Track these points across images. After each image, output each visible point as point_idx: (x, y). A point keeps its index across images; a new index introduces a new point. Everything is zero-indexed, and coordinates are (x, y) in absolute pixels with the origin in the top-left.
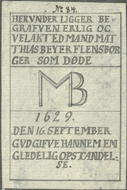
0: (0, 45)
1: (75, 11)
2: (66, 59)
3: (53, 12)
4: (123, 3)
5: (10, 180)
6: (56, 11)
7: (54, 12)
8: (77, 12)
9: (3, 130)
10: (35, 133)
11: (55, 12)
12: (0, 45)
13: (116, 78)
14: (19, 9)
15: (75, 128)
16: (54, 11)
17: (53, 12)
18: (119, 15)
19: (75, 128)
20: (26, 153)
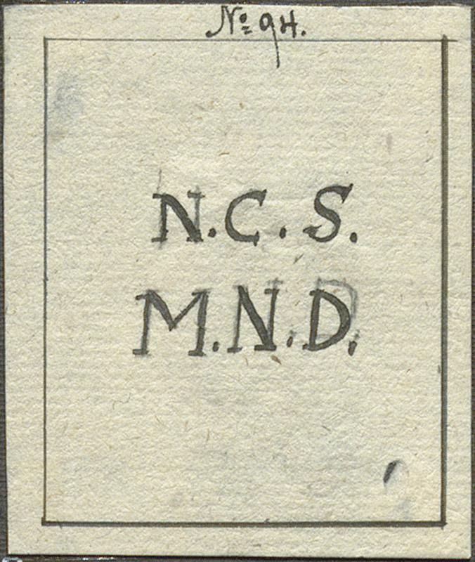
0: (2, 476)
1: (299, 29)
2: (319, 345)
3: (206, 38)
4: (440, 460)
5: (45, 40)
6: (220, 30)
7: (214, 37)
8: (304, 33)
9: (40, 203)
10: (222, 305)
11: (215, 34)
12: (2, 476)
13: (391, 341)
14: (38, 346)
15: (312, 297)
16: (213, 32)
17: (209, 34)
18: (437, 518)
19: (312, 297)
20: (158, 201)
